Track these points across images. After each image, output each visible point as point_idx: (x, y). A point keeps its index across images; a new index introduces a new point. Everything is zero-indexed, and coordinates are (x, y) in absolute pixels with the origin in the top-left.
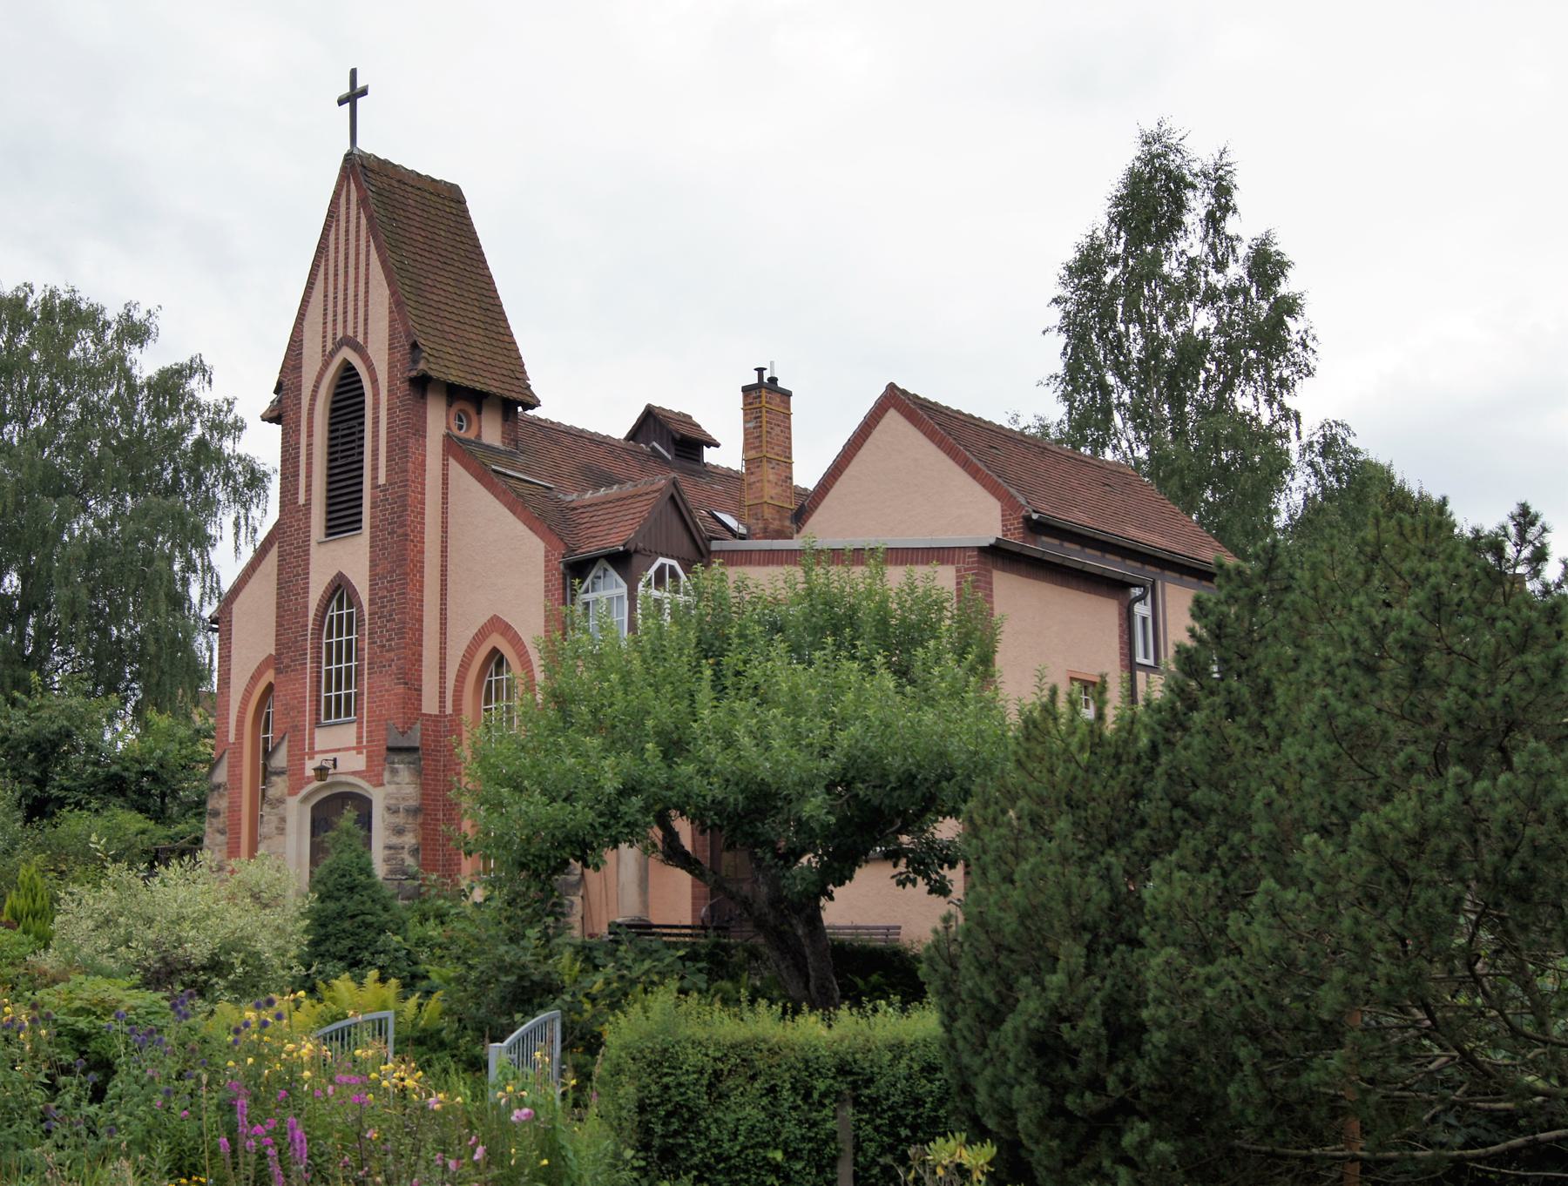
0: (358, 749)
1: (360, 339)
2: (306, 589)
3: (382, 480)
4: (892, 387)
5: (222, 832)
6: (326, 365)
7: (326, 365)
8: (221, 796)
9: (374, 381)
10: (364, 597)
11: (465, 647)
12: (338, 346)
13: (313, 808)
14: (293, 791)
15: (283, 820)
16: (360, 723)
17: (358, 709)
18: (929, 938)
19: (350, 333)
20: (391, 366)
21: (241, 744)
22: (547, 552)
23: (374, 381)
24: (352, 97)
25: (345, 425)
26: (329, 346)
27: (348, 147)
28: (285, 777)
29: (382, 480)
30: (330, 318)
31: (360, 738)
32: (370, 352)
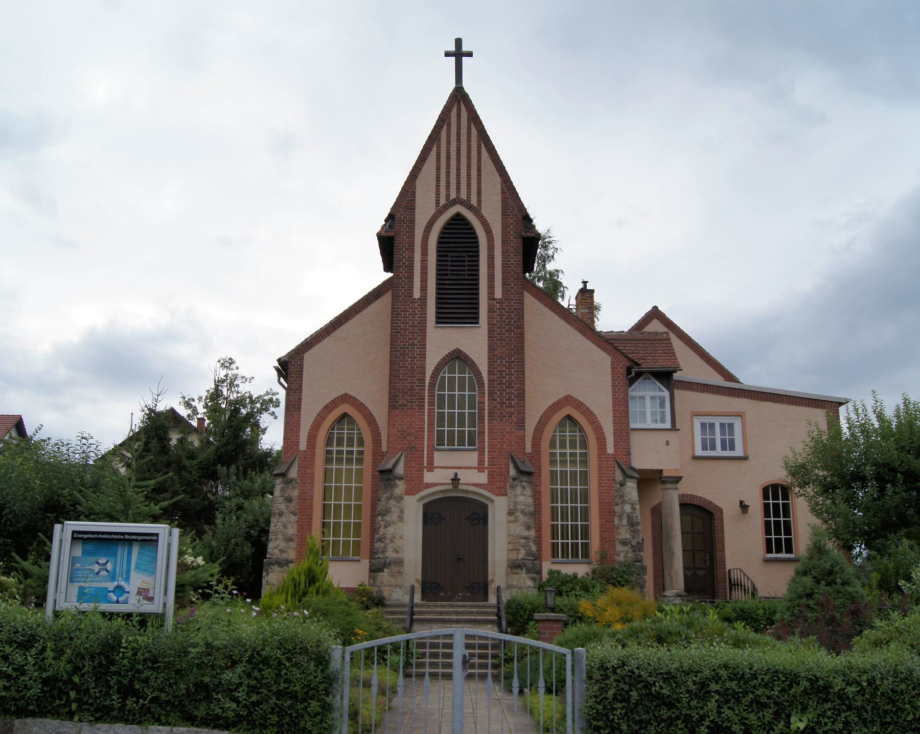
0: (480, 468)
1: (474, 202)
2: (423, 356)
3: (498, 294)
4: (655, 308)
5: (294, 514)
6: (440, 212)
7: (440, 212)
8: (294, 487)
9: (489, 232)
10: (484, 368)
11: (542, 411)
12: (451, 203)
13: (424, 505)
14: (410, 492)
15: (402, 511)
16: (481, 452)
17: (482, 441)
18: (785, 592)
19: (464, 196)
20: (505, 227)
21: (313, 454)
22: (613, 364)
23: (489, 232)
24: (459, 54)
25: (455, 254)
26: (443, 201)
27: (452, 85)
28: (403, 481)
29: (498, 294)
30: (443, 183)
31: (481, 461)
32: (484, 212)
